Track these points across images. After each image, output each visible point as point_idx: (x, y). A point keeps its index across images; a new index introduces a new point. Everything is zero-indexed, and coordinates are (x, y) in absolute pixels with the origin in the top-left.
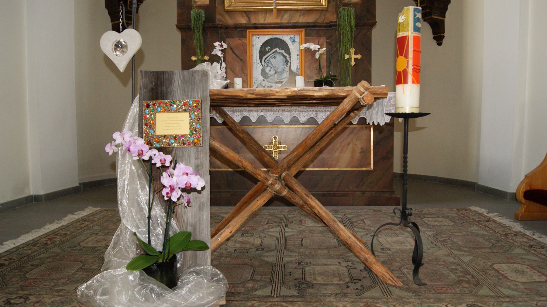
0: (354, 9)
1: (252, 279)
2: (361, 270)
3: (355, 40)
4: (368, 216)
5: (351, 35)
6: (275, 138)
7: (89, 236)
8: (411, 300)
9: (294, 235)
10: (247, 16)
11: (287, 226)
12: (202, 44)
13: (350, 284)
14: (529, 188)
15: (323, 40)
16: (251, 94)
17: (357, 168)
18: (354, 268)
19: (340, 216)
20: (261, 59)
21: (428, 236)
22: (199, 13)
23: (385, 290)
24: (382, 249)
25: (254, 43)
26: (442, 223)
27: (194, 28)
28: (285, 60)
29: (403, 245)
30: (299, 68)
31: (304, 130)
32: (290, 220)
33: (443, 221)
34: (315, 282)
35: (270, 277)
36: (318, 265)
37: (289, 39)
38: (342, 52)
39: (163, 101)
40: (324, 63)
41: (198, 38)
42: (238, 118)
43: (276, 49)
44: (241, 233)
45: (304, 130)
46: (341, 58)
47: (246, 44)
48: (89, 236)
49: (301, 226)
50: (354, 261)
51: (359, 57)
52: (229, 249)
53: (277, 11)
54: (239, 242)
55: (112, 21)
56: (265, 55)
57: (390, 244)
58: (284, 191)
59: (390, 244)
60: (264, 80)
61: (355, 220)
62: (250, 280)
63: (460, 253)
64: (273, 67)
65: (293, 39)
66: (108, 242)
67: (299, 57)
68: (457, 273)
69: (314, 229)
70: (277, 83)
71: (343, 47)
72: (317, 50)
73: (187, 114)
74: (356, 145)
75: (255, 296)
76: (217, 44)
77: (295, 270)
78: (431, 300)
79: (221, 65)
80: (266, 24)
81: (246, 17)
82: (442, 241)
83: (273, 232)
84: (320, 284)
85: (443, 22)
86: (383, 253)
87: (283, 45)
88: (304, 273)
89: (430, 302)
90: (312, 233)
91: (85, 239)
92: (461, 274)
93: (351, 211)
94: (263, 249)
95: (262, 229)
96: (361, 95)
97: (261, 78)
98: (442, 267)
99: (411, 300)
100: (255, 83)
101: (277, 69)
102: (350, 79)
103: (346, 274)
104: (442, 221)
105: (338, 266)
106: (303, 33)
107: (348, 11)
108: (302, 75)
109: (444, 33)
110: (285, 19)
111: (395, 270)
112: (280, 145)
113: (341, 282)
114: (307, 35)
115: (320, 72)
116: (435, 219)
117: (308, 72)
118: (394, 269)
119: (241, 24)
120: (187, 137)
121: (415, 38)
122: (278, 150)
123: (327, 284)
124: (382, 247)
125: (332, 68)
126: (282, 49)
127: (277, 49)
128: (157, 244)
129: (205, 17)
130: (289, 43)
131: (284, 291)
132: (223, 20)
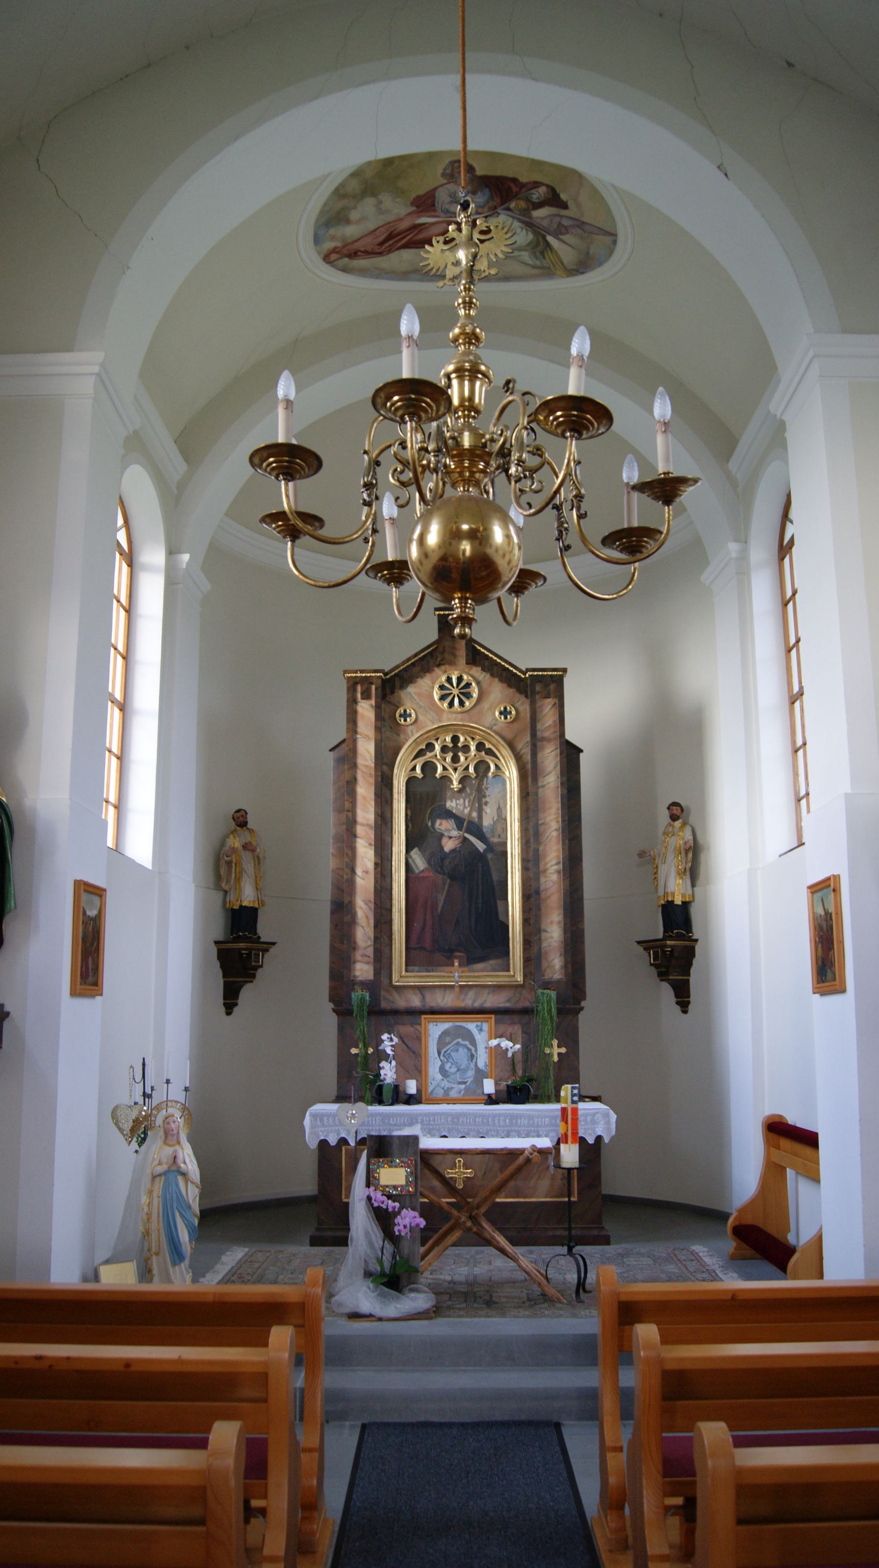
1: (450, 1300)
11: (475, 1266)
14: (738, 1223)
20: (439, 1053)
25: (431, 1032)
27: (356, 1016)
28: (469, 1054)
43: (458, 1040)
47: (420, 1032)
51: (563, 1050)
54: (430, 1279)
55: (224, 976)
56: (444, 1048)
64: (455, 1063)
70: (460, 1083)
81: (419, 995)
88: (491, 1296)
97: (439, 1077)
109: (689, 996)
110: (469, 1000)
126: (466, 1040)
127: (460, 1040)
128: (387, 1266)
130: (475, 1032)
131: (475, 1305)
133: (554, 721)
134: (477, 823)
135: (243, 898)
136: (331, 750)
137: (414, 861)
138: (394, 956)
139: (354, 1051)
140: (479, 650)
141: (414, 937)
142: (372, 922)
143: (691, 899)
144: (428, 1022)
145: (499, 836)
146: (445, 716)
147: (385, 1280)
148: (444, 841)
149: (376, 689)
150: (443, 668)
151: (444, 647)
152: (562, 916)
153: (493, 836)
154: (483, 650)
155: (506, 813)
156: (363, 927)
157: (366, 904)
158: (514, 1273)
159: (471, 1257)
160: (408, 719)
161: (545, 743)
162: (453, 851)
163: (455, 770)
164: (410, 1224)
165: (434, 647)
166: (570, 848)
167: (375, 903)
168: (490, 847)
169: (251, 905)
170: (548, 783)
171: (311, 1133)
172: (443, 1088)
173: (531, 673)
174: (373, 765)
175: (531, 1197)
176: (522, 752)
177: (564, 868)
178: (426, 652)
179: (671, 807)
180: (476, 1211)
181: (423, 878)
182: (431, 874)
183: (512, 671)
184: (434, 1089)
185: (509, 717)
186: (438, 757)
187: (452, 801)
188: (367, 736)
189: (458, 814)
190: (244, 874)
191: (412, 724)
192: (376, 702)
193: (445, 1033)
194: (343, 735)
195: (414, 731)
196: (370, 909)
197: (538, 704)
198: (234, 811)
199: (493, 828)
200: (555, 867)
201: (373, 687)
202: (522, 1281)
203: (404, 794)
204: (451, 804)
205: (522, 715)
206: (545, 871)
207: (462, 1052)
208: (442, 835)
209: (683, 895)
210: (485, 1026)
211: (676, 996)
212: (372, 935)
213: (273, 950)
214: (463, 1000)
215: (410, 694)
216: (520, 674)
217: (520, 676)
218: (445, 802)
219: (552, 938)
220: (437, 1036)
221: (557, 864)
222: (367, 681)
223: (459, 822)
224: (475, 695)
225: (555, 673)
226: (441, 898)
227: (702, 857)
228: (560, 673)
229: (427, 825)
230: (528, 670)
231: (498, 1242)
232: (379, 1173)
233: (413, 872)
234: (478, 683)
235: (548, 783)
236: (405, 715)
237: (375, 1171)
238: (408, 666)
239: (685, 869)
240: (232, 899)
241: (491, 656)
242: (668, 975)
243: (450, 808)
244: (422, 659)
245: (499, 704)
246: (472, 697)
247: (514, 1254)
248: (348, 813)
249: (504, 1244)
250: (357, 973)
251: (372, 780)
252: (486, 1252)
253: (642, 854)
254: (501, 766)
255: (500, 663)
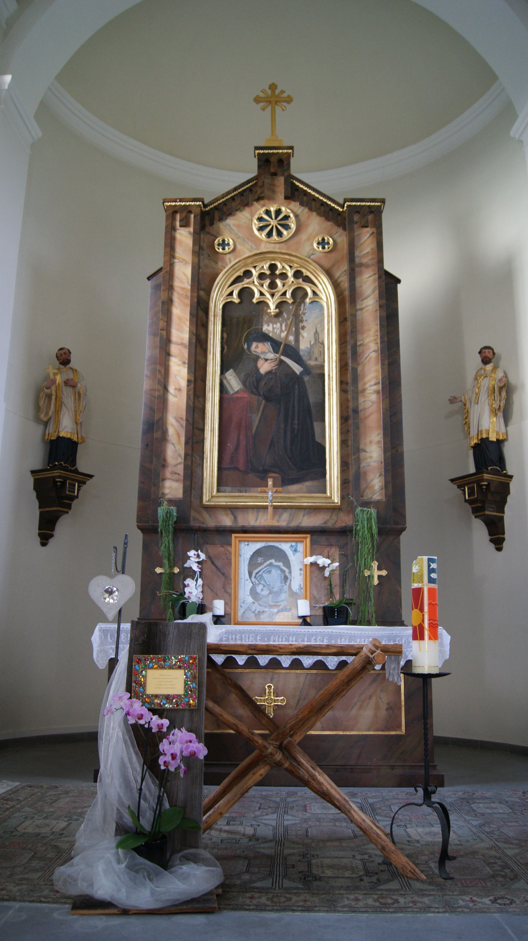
0: (376, 511)
1: (247, 871)
2: (379, 864)
3: (378, 550)
4: (398, 801)
5: (373, 545)
6: (270, 687)
7: (23, 820)
8: (432, 893)
9: (296, 824)
10: (233, 514)
11: (286, 813)
12: (172, 553)
13: (364, 878)
15: (335, 552)
16: (252, 649)
17: (383, 731)
18: (371, 861)
19: (359, 801)
20: (250, 576)
21: (473, 826)
22: (170, 512)
23: (405, 884)
24: (408, 841)
25: (242, 552)
26: (495, 811)
28: (283, 576)
29: (437, 836)
30: (302, 587)
31: (309, 677)
32: (290, 805)
33: (498, 807)
34: (322, 875)
35: (269, 869)
36: (328, 858)
37: (290, 548)
38: (360, 568)
39: (155, 656)
40: (336, 581)
41: (167, 544)
42: (219, 659)
43: (271, 561)
44: (226, 821)
45: (309, 677)
46: (359, 576)
47: (230, 553)
48: (24, 820)
49: (305, 813)
50: (372, 854)
51: (384, 573)
52: (214, 840)
53: (274, 508)
54: (226, 831)
55: (40, 507)
57: (420, 836)
58: (286, 763)
59: (420, 836)
60: (254, 603)
61: (378, 806)
62: (246, 872)
63: (506, 845)
65: (295, 547)
66: (53, 828)
67: (302, 572)
68: (494, 867)
69: (323, 816)
71: (362, 560)
72: (327, 566)
73: (181, 672)
74: (380, 699)
75: (254, 888)
76: (192, 553)
77: (299, 863)
78: (455, 893)
79: (197, 583)
80: (257, 527)
81: (232, 517)
82: (488, 833)
83: (268, 819)
84: (329, 877)
85: (502, 519)
86: (409, 845)
87: (282, 556)
88: (309, 865)
89: (453, 895)
90: (320, 822)
91: (21, 824)
92: (499, 868)
93: (374, 794)
94: (258, 840)
95: (253, 816)
96: (372, 654)
97: (250, 600)
98: (478, 860)
99: (432, 893)
100: (241, 607)
101: (273, 588)
102: (372, 604)
103: (361, 867)
104: (496, 808)
105: (351, 860)
106: (308, 540)
107: (368, 513)
108: (306, 599)
109: (503, 533)
110: (283, 521)
111: (422, 864)
112: (277, 697)
113: (354, 876)
114: (312, 543)
115: (331, 593)
116: (487, 805)
117: (315, 593)
118: (419, 862)
119: (225, 527)
120: (181, 697)
121: (430, 590)
122: (273, 704)
123: (338, 877)
124: (409, 839)
125: (347, 588)
126: (279, 561)
127: (273, 561)
128: (146, 823)
129: (177, 517)
131: (287, 883)
132: (201, 519)
133: (372, 249)
134: (294, 347)
135: (61, 429)
136: (149, 279)
137: (229, 383)
138: (205, 475)
139: (158, 570)
140: (298, 186)
141: (227, 457)
142: (183, 439)
143: (505, 437)
144: (239, 541)
145: (316, 359)
146: (263, 245)
147: (141, 842)
148: (260, 363)
149: (194, 217)
150: (262, 202)
151: (263, 182)
152: (381, 435)
153: (310, 359)
154: (301, 186)
155: (324, 338)
156: (173, 444)
157: (178, 421)
158: (337, 824)
159: (282, 800)
160: (226, 248)
161: (363, 268)
162: (269, 373)
163: (273, 295)
164: (182, 752)
165: (253, 183)
166: (389, 372)
167: (187, 420)
168: (307, 370)
169: (69, 436)
170: (368, 306)
171: (100, 651)
172: (254, 612)
173: (349, 203)
174: (189, 287)
175: (352, 730)
176: (340, 280)
177: (383, 388)
178: (245, 187)
179: (483, 351)
180: (289, 739)
181: (238, 398)
182: (246, 395)
183: (330, 205)
184: (244, 612)
185: (326, 246)
186: (256, 283)
187: (268, 326)
188: (184, 260)
189: (274, 337)
190: (63, 407)
191: (229, 253)
192: (194, 229)
193: (257, 553)
194: (160, 265)
195: (232, 259)
196: (182, 426)
197: (356, 233)
198: (58, 349)
199: (310, 352)
200: (375, 388)
201: (192, 216)
202: (350, 838)
203: (220, 317)
204: (267, 328)
205: (340, 246)
206: (364, 390)
207: (275, 574)
208: (257, 358)
209: (498, 434)
210: (301, 547)
211: (490, 534)
212: (183, 453)
213: (89, 482)
214: (278, 521)
215: (229, 226)
216: (337, 208)
217: (338, 210)
218: (262, 326)
219: (371, 457)
220: (249, 557)
221: (375, 384)
222: (188, 210)
223: (276, 344)
224: (293, 226)
225: (373, 204)
226: (256, 419)
227: (516, 398)
228: (379, 204)
229: (243, 348)
230: (346, 200)
231: (320, 783)
232: (145, 677)
233: (227, 392)
234: (296, 216)
235: (368, 306)
236: (223, 244)
237: (138, 673)
238: (227, 200)
239: (500, 406)
240: (50, 432)
241: (309, 191)
242: (484, 510)
243: (267, 332)
244: (242, 194)
245: (317, 235)
246: (290, 228)
247: (343, 802)
248: (162, 332)
249: (329, 787)
250: (166, 491)
251: (188, 302)
252: (299, 794)
253: (453, 400)
254: (318, 292)
255: (318, 198)
